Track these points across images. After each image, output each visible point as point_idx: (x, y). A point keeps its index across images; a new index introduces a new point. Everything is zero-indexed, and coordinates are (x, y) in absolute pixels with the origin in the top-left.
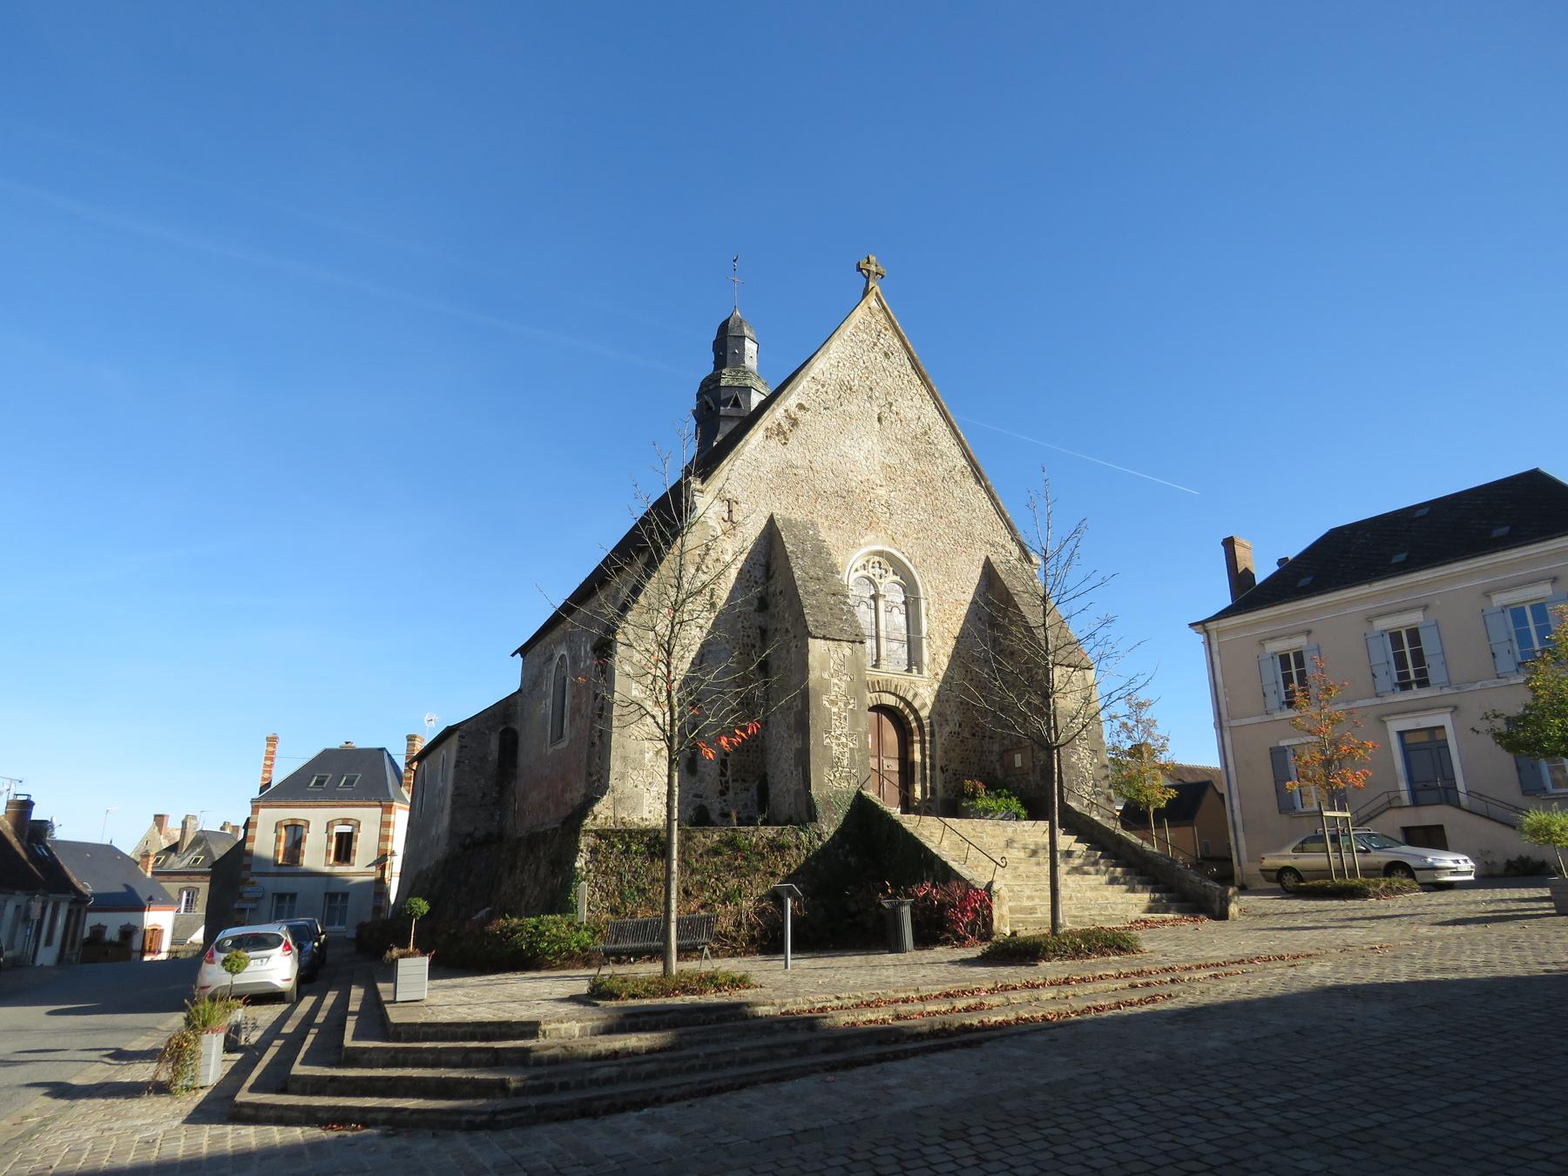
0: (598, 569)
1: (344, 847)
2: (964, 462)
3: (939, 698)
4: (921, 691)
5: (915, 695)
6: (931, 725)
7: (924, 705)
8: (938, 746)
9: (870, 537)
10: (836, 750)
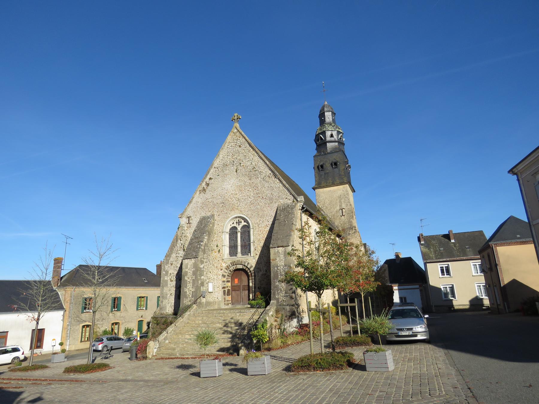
0: (28, 282)
1: (38, 337)
2: (270, 172)
3: (258, 263)
4: (250, 262)
5: (248, 263)
6: (254, 273)
7: (252, 266)
8: (257, 280)
9: (233, 212)
10: (188, 293)
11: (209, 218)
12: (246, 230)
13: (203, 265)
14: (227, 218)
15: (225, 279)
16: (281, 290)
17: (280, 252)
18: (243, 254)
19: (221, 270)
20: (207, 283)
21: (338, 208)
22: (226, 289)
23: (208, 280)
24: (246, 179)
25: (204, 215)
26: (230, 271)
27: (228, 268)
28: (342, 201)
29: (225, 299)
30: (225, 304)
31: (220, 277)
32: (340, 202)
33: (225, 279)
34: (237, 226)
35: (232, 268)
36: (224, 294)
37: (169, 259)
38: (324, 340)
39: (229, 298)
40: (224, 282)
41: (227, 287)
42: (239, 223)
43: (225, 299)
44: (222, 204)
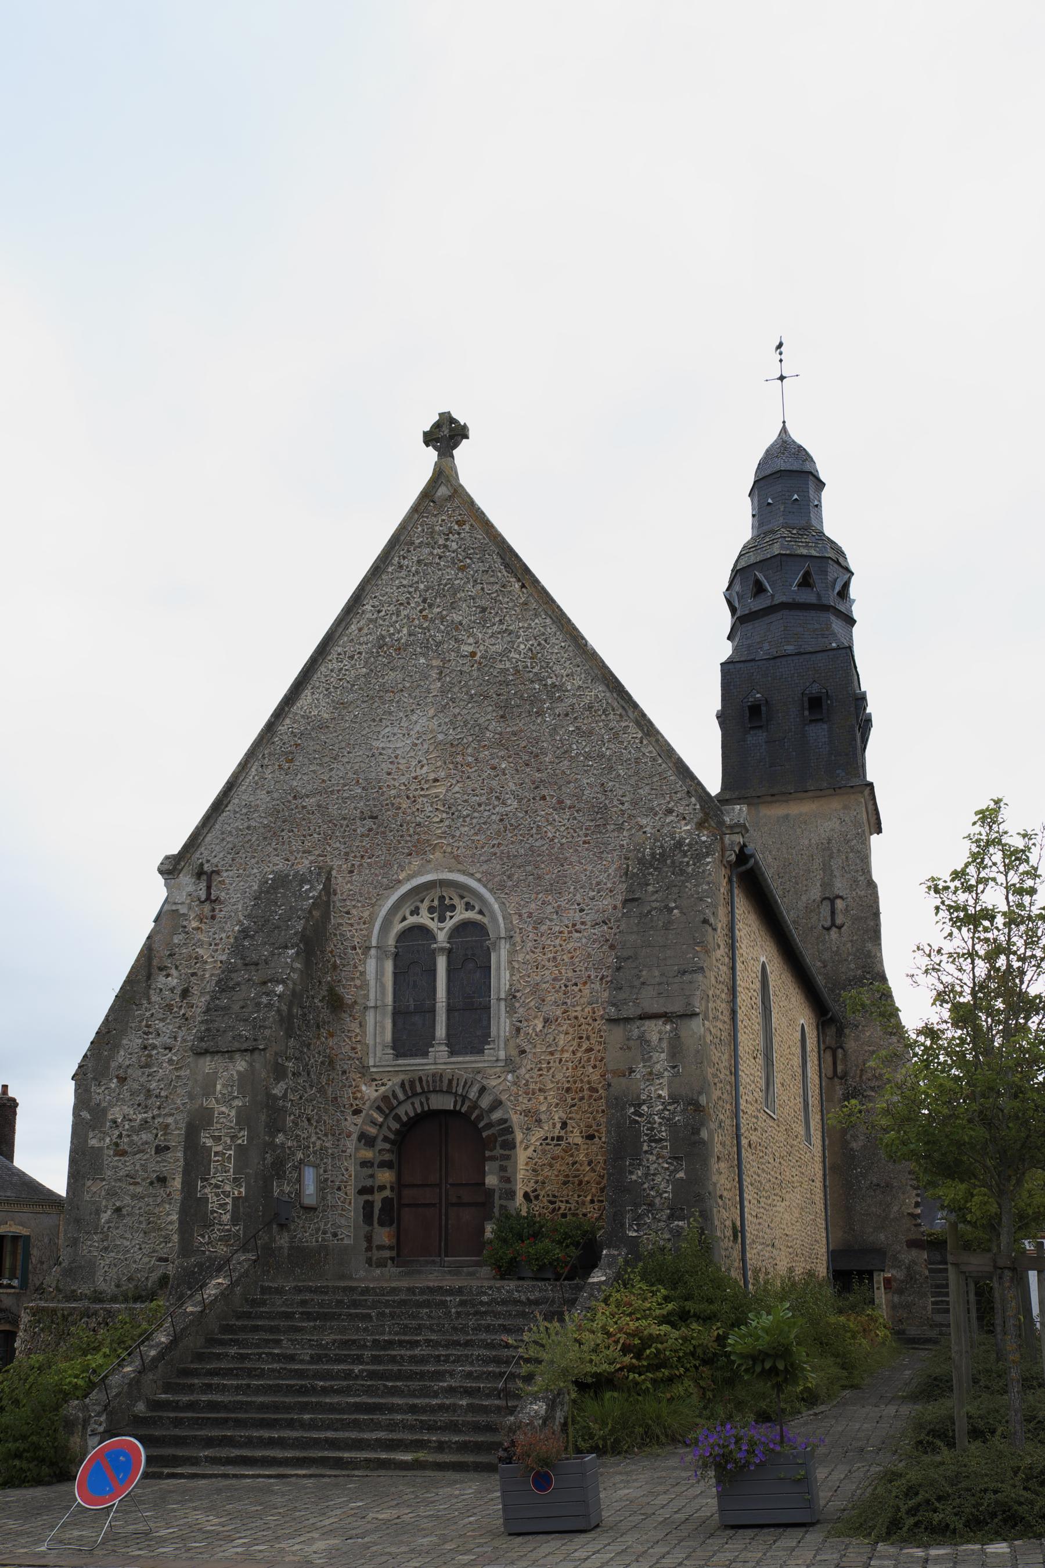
5: (483, 1090)
9: (416, 862)
11: (303, 881)
12: (472, 948)
13: (282, 1085)
14: (388, 888)
15: (368, 1154)
16: (651, 1204)
17: (654, 1038)
18: (454, 1047)
19: (357, 1112)
20: (298, 1167)
21: (816, 893)
22: (377, 1198)
23: (300, 1155)
24: (488, 716)
25: (281, 866)
26: (397, 1118)
27: (386, 1105)
28: (836, 863)
29: (369, 1239)
30: (369, 1261)
31: (351, 1144)
32: (826, 868)
33: (368, 1154)
34: (433, 925)
35: (406, 1111)
36: (368, 1217)
37: (111, 1058)
38: (192, 1362)
39: (383, 1235)
40: (364, 1164)
41: (382, 1188)
42: (442, 910)
43: (369, 1239)
44: (369, 823)
